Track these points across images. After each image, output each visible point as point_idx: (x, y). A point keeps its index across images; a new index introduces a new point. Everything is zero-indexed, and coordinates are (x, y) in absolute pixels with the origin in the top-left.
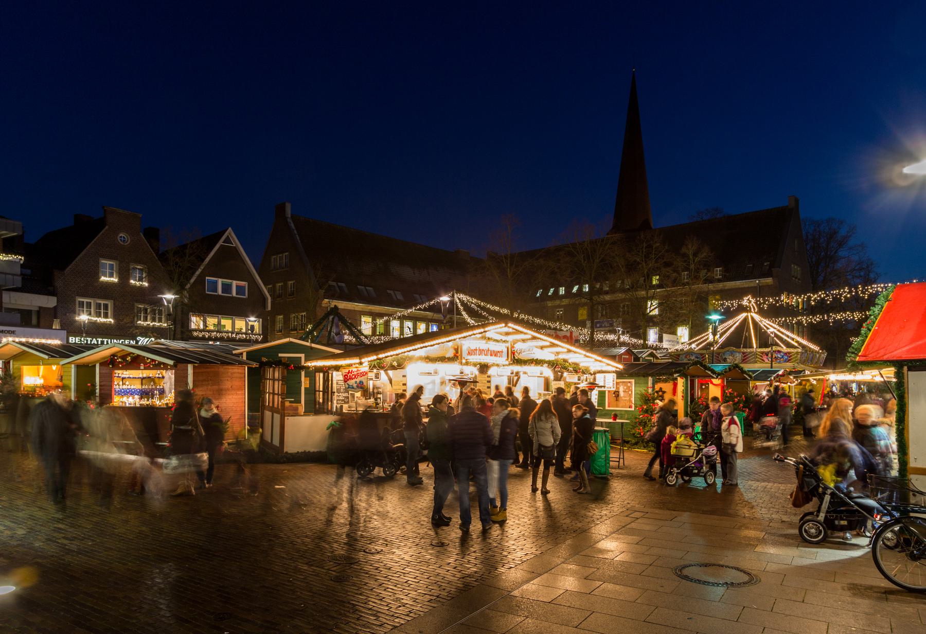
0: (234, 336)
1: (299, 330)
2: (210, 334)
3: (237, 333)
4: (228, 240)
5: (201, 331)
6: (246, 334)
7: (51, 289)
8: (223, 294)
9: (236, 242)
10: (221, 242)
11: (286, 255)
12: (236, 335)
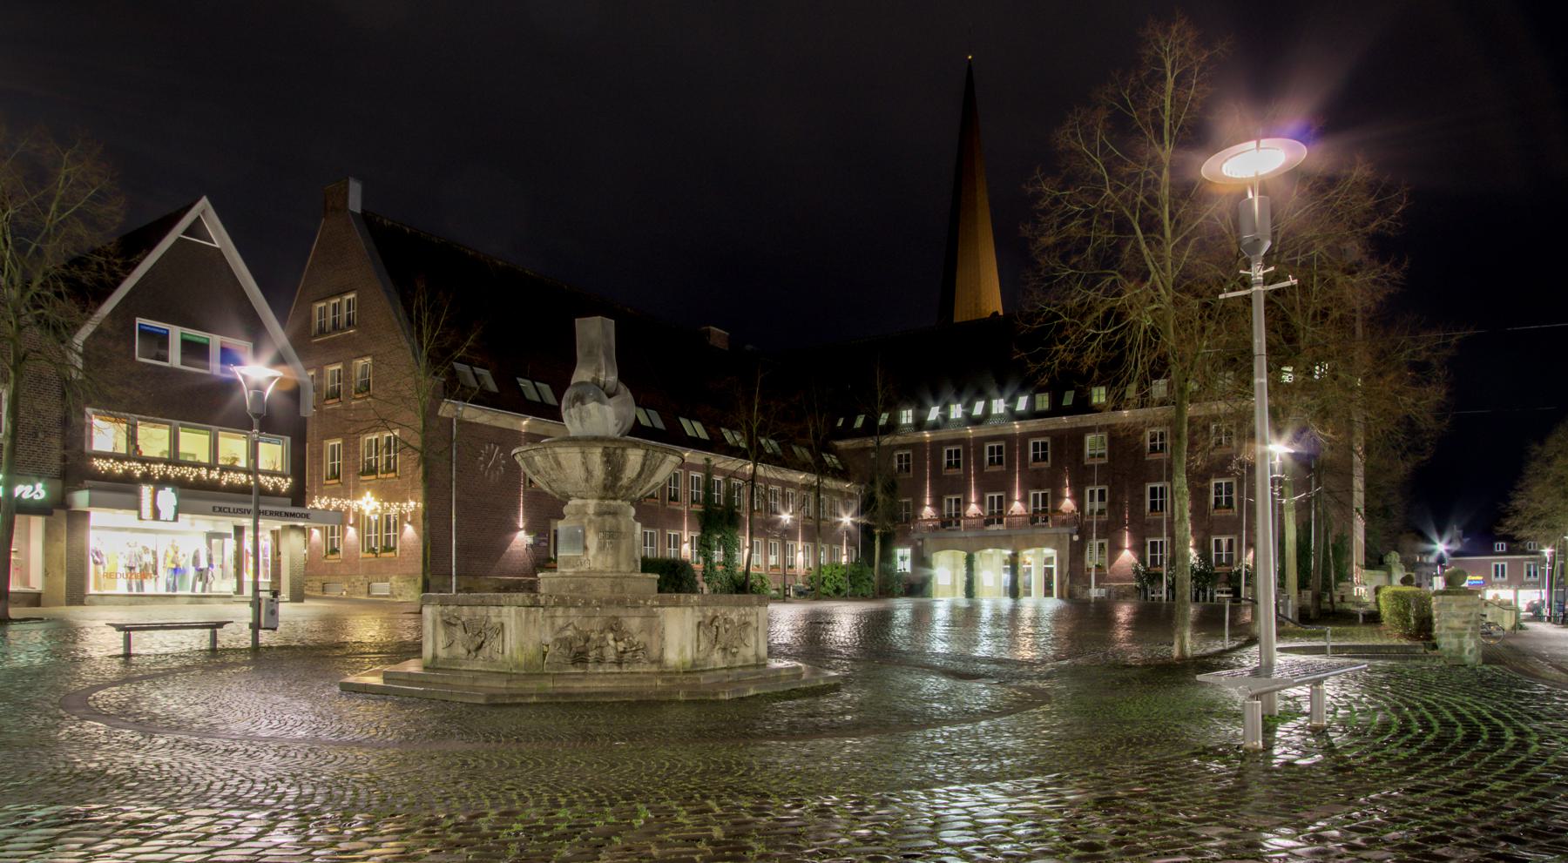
0: (215, 475)
1: (382, 473)
2: (148, 468)
3: (225, 469)
4: (196, 229)
5: (119, 458)
6: (247, 471)
7: (162, 352)
8: (1107, 499)
9: (219, 237)
10: (178, 231)
11: (349, 301)
12: (221, 474)
